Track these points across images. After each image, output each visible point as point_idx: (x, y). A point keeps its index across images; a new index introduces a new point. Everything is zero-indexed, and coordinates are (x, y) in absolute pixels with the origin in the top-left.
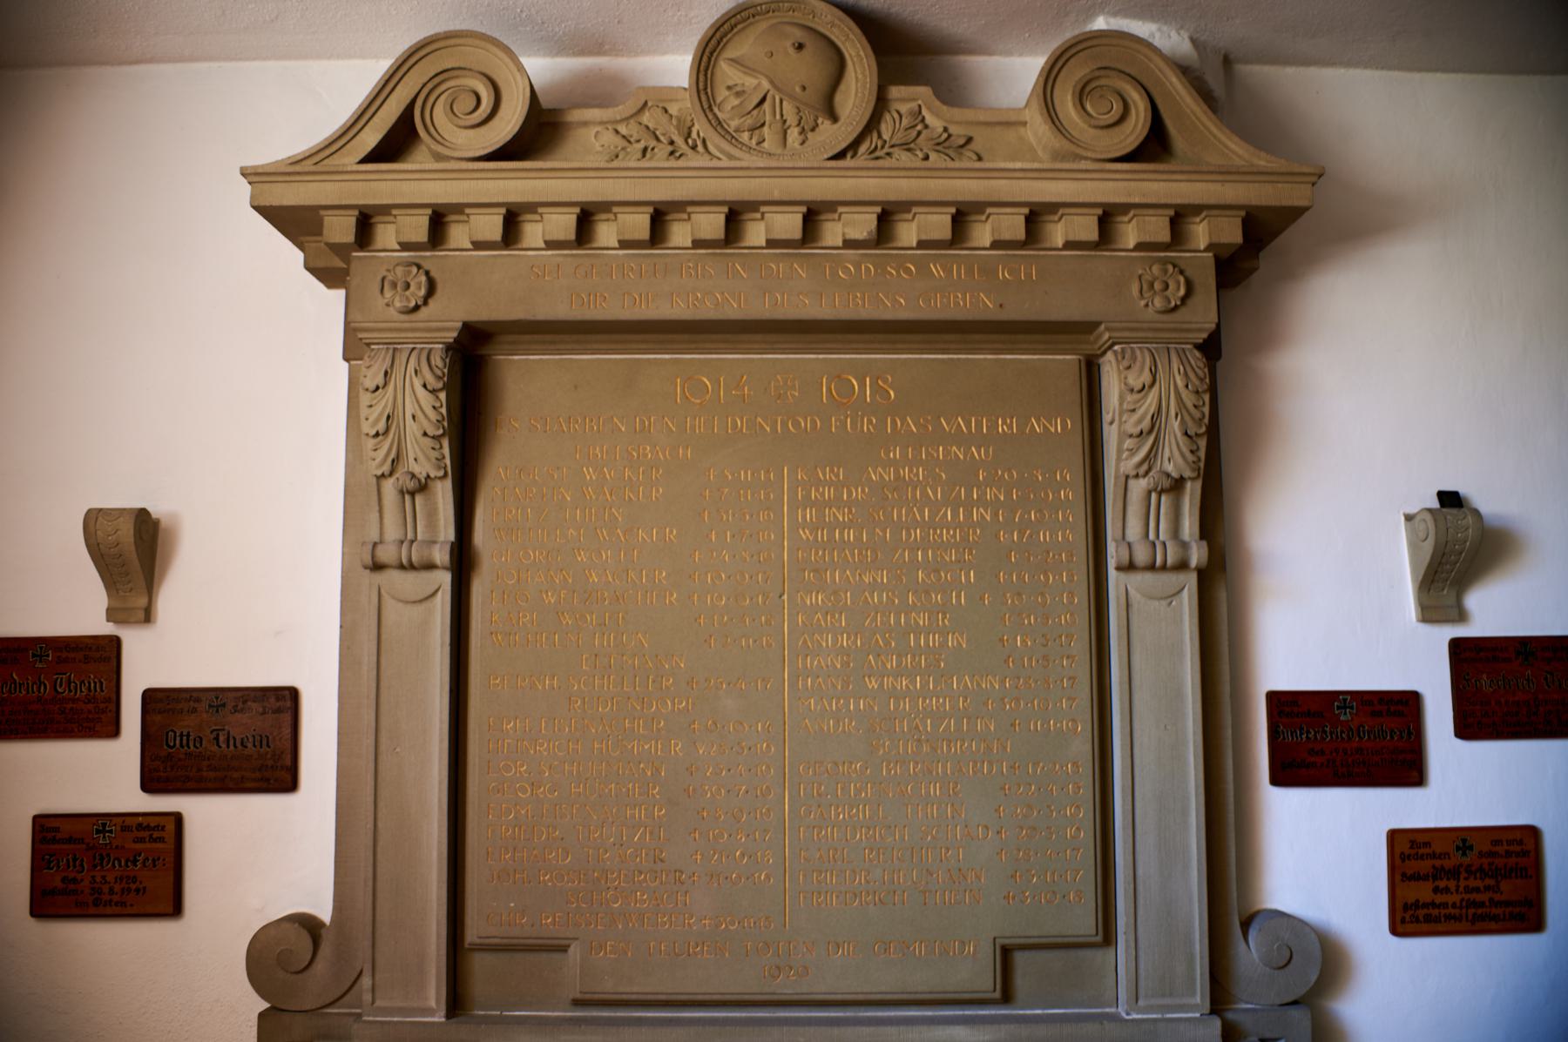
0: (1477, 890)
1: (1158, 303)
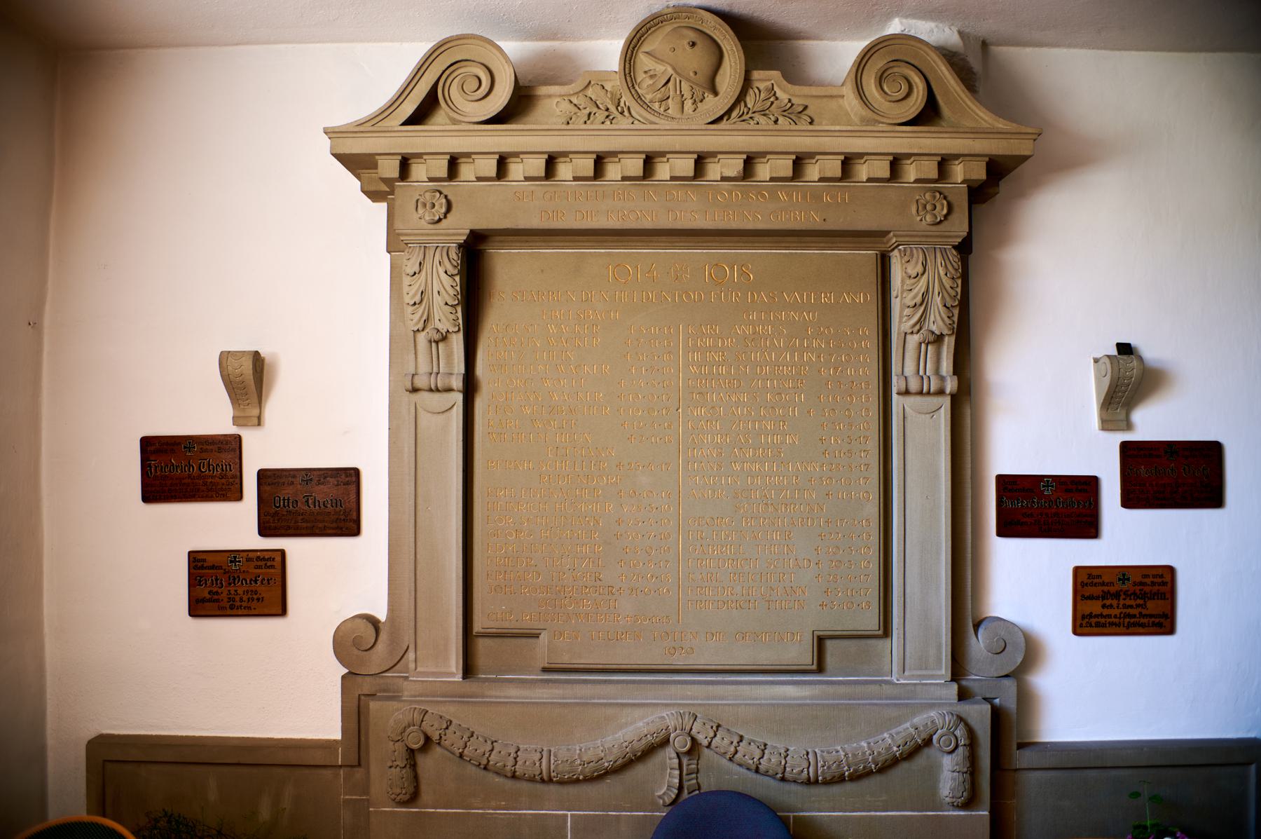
0: (1131, 607)
1: (929, 218)
